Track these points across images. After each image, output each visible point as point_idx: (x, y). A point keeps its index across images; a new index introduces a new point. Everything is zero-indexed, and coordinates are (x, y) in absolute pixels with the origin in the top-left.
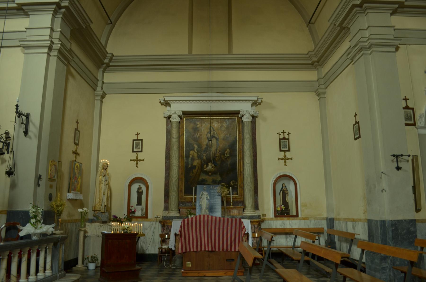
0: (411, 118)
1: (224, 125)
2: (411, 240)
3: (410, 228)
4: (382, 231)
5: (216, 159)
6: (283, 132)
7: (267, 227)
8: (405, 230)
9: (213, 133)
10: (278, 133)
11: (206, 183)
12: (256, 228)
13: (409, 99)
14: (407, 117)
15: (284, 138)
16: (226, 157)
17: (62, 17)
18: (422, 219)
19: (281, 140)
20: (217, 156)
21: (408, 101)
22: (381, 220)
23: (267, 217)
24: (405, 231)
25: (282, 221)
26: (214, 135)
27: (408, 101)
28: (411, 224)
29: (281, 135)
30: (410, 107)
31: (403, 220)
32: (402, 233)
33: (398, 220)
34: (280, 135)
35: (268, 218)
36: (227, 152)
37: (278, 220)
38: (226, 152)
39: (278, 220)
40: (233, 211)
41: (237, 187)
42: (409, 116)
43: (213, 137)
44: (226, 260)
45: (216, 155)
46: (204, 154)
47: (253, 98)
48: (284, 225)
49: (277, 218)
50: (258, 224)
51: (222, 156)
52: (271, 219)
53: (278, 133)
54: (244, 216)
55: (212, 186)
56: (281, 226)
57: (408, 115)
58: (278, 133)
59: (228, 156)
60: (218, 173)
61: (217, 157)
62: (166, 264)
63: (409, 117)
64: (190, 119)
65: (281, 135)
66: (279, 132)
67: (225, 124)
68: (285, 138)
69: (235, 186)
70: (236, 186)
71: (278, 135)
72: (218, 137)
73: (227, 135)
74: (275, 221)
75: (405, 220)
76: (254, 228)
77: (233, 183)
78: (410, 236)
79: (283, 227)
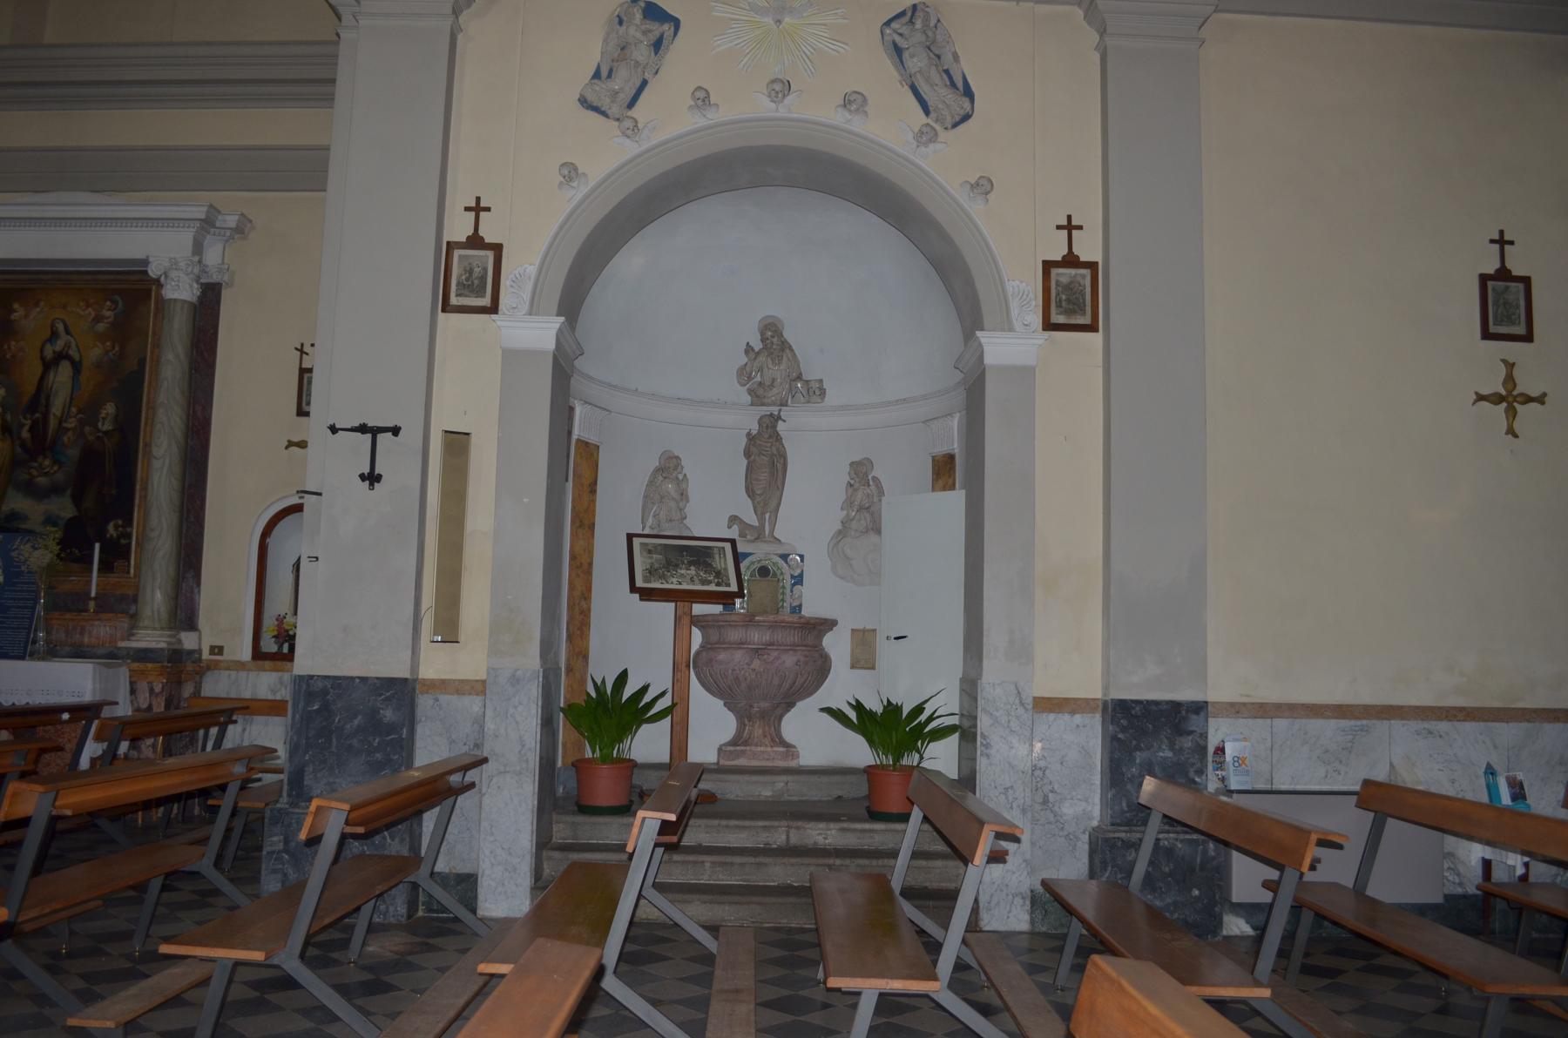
0: (486, 283)
1: (108, 313)
2: (379, 756)
3: (381, 711)
4: (297, 716)
5: (65, 439)
7: (223, 695)
8: (360, 717)
9: (65, 345)
10: (297, 349)
11: (23, 526)
12: (157, 695)
14: (467, 280)
16: (100, 434)
20: (68, 429)
21: (1507, 247)
23: (227, 656)
25: (280, 674)
26: (67, 352)
27: (1507, 247)
28: (388, 694)
30: (487, 241)
31: (357, 680)
34: (304, 356)
35: (227, 661)
36: (107, 414)
38: (103, 415)
40: (95, 631)
41: (130, 544)
43: (61, 356)
44: (1487, 857)
45: (65, 425)
46: (25, 418)
47: (184, 211)
48: (283, 689)
50: (165, 681)
51: (87, 429)
52: (240, 666)
54: (120, 648)
55: (20, 538)
56: (274, 692)
57: (471, 272)
58: (297, 349)
59: (110, 428)
60: (69, 492)
61: (70, 434)
62: (1131, 856)
63: (476, 282)
65: (307, 354)
66: (302, 345)
67: (109, 310)
69: (123, 541)
70: (127, 541)
71: (299, 353)
72: (81, 357)
73: (114, 352)
74: (252, 675)
75: (364, 679)
76: (150, 697)
77: (116, 527)
78: (374, 739)
79: (281, 695)
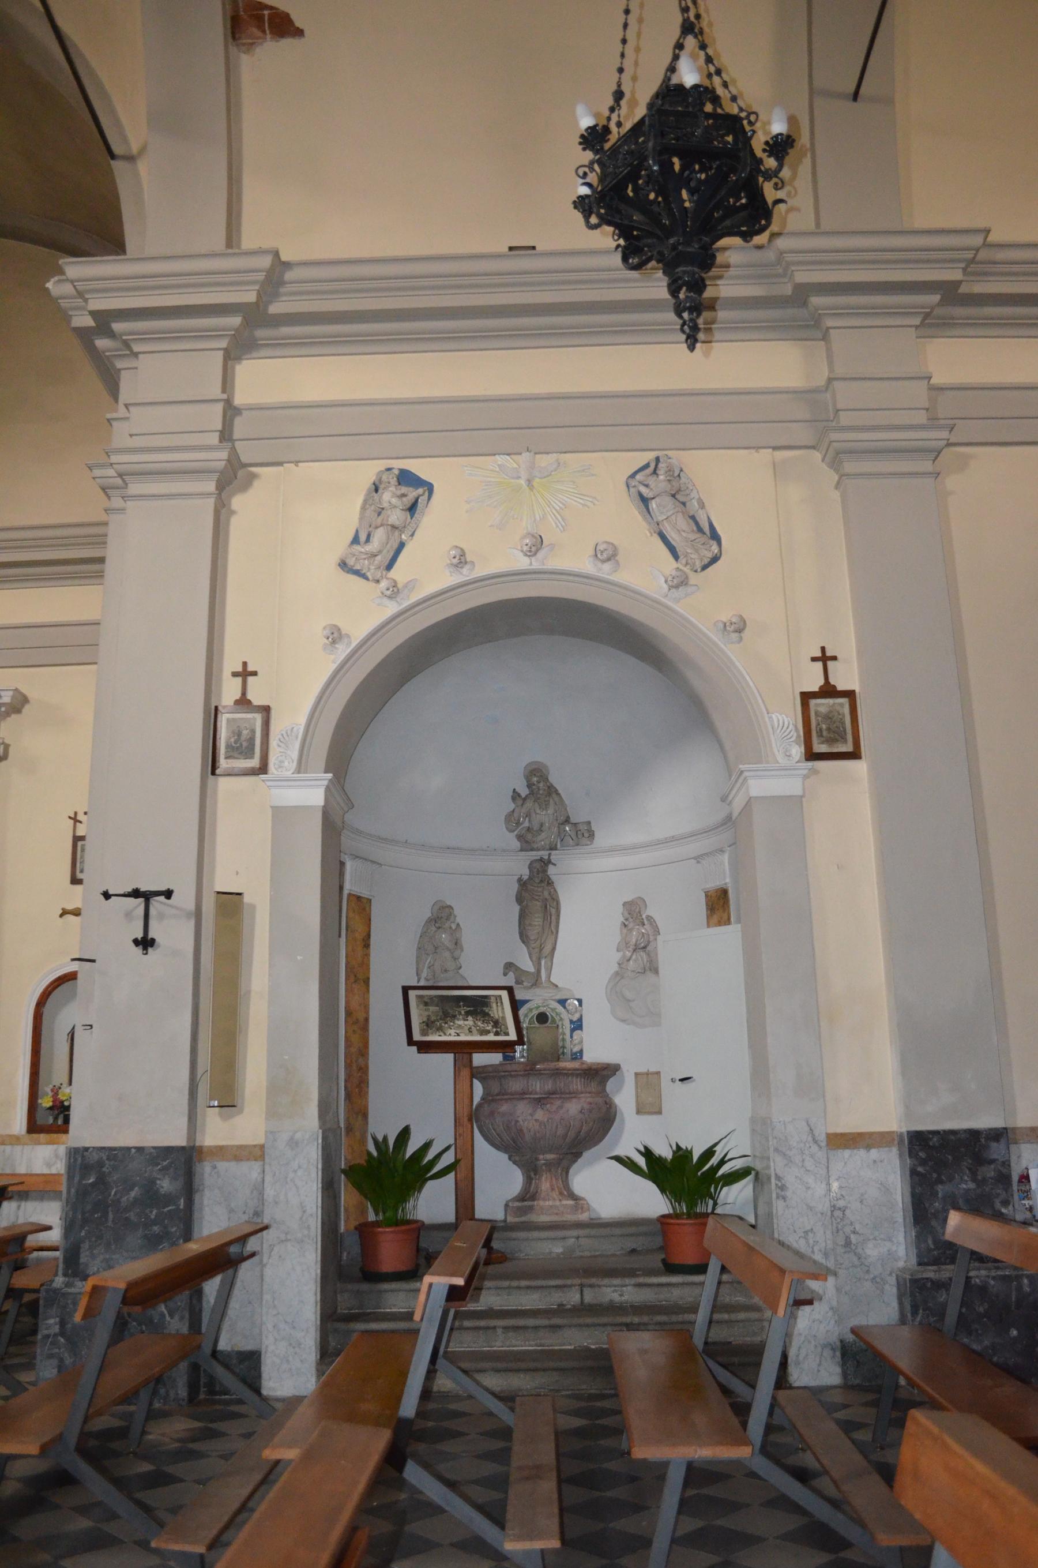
2: (156, 1229)
3: (158, 1182)
4: (73, 1190)
6: (819, 654)
10: (70, 818)
13: (259, 673)
14: (235, 742)
15: (828, 691)
17: (258, 290)
18: (241, 1147)
19: (813, 702)
22: (74, 1148)
24: (133, 1194)
25: (55, 1146)
28: (165, 1163)
29: (80, 822)
32: (124, 1199)
33: (111, 1149)
34: (78, 824)
37: (38, 1143)
39: (39, 1144)
42: (243, 738)
49: (35, 1136)
53: (73, 816)
56: (49, 1165)
57: (239, 734)
58: (70, 818)
63: (245, 744)
64: (210, 717)
65: (80, 822)
66: (76, 813)
68: (834, 686)
74: (27, 1149)
75: (140, 1150)
78: (151, 1212)
